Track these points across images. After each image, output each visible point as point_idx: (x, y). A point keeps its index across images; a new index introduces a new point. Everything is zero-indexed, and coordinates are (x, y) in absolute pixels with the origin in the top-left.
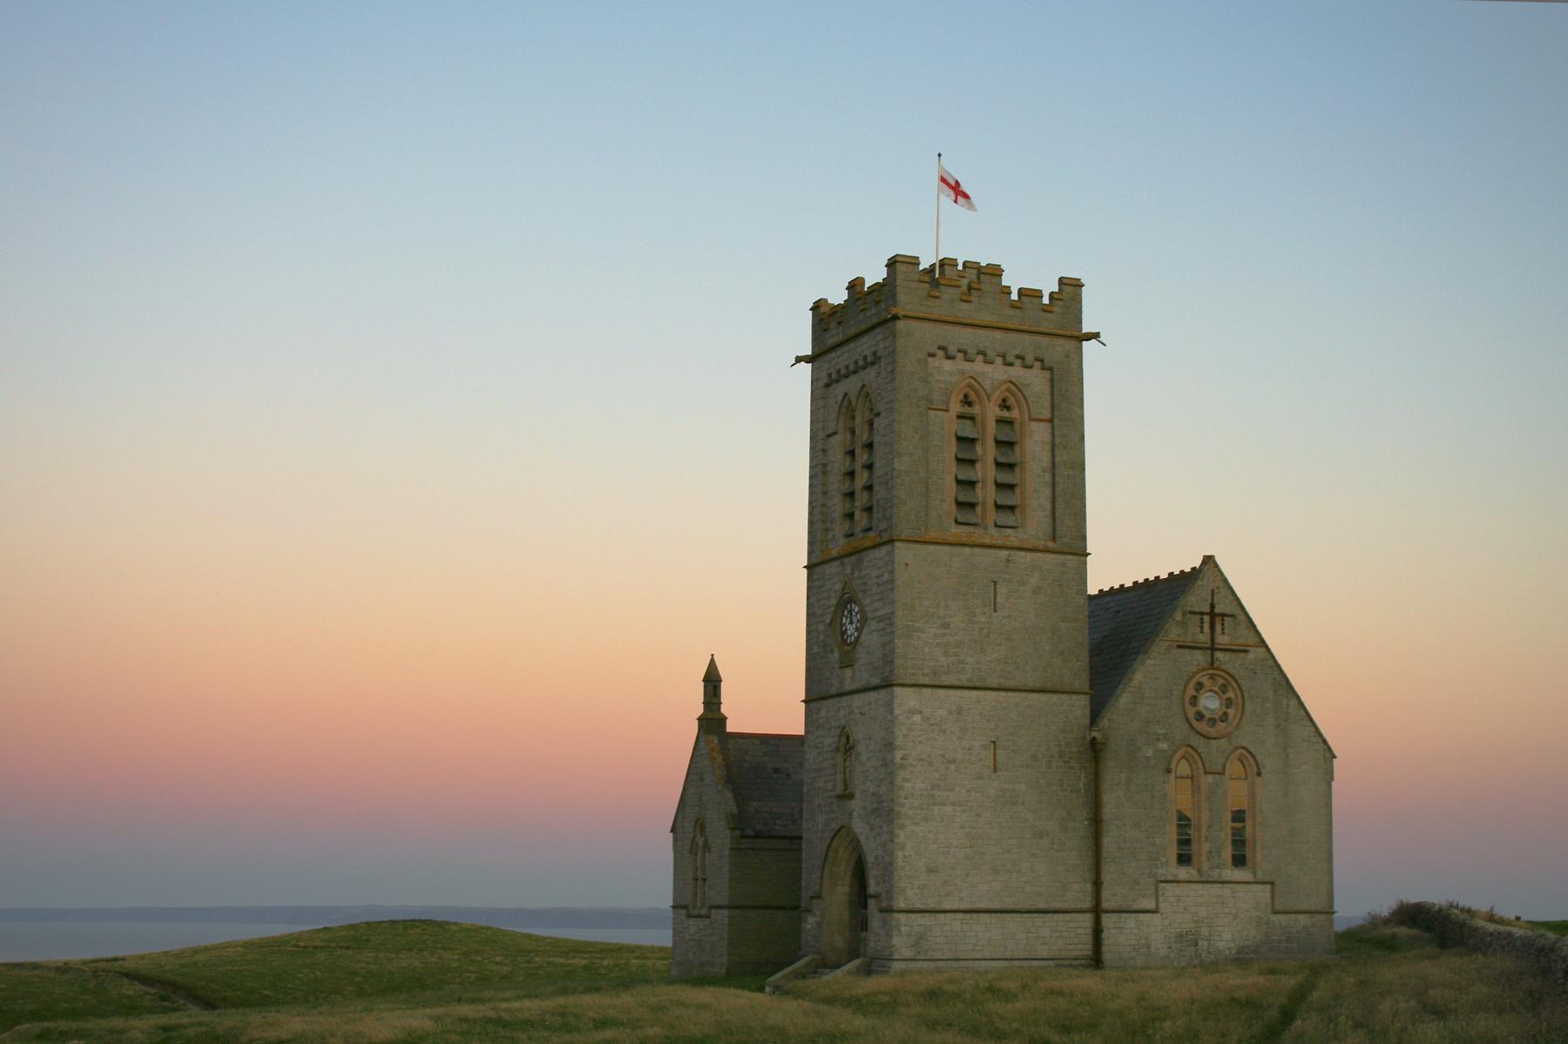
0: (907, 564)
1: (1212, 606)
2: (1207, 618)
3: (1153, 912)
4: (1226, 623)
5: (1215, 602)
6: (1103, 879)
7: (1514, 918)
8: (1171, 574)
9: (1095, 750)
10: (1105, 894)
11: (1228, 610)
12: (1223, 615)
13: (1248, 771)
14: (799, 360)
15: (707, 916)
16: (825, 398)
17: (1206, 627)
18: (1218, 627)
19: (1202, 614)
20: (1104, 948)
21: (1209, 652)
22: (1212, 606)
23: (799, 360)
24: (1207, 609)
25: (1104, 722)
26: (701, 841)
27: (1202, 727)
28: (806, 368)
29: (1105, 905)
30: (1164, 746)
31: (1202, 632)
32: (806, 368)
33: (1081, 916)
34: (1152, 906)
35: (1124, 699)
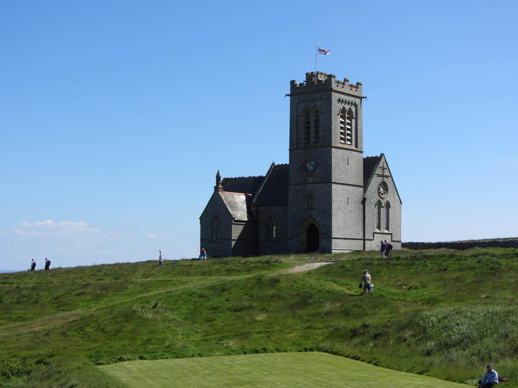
2: (382, 169)
3: (372, 240)
11: (386, 167)
12: (385, 168)
14: (287, 95)
23: (287, 95)
34: (372, 238)
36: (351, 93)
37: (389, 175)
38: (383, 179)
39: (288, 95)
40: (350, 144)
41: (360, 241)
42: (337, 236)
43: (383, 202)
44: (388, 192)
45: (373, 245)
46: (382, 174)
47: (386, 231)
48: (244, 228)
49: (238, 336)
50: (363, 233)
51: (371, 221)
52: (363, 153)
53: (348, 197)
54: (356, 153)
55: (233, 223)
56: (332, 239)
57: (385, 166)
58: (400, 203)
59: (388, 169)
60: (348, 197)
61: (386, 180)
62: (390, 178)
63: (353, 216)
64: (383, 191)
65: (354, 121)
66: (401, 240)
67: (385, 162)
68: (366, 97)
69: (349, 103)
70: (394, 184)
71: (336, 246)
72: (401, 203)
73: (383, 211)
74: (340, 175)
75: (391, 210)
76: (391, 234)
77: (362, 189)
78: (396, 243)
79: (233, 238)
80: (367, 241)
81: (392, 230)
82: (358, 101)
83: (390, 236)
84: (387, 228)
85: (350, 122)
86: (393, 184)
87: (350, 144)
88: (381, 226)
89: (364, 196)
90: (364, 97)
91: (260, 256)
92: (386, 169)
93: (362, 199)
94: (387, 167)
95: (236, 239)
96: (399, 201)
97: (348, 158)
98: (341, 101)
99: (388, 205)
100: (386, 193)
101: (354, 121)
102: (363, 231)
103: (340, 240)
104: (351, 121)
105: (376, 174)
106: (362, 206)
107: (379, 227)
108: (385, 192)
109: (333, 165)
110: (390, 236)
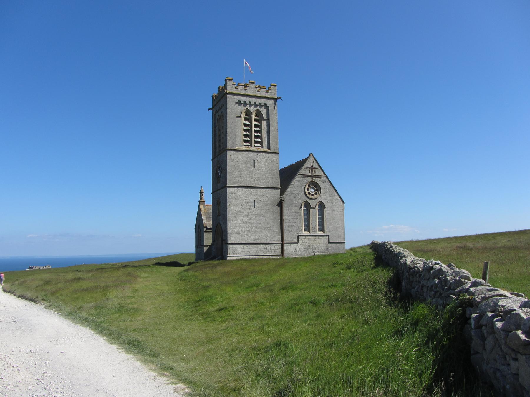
0: (230, 156)
1: (312, 166)
2: (311, 169)
3: (297, 243)
4: (316, 170)
5: (313, 165)
6: (284, 235)
7: (38, 269)
8: (303, 159)
9: (280, 204)
10: (285, 238)
11: (316, 167)
12: (315, 168)
13: (322, 207)
14: (209, 109)
15: (201, 248)
16: (460, 238)
17: (310, 171)
18: (314, 171)
19: (309, 168)
20: (285, 252)
21: (311, 178)
22: (312, 166)
23: (209, 109)
24: (310, 167)
25: (284, 195)
26: (199, 230)
27: (310, 196)
28: (211, 111)
29: (285, 241)
30: (300, 201)
31: (309, 172)
32: (211, 111)
33: (276, 246)
34: (297, 242)
35: (289, 189)
36: (259, 94)
37: (322, 174)
38: (312, 179)
39: (211, 109)
40: (260, 145)
41: (275, 245)
42: (237, 242)
43: (313, 203)
44: (320, 193)
45: (298, 249)
46: (310, 174)
47: (321, 233)
48: (212, 235)
49: (257, 323)
50: (280, 237)
51: (295, 223)
52: (279, 154)
53: (254, 201)
54: (269, 154)
55: (205, 231)
56: (228, 246)
57: (315, 165)
58: (341, 202)
59: (320, 169)
60: (254, 201)
61: (316, 180)
62: (325, 178)
63: (264, 219)
64: (315, 191)
65: (264, 123)
66: (344, 240)
67: (315, 162)
68: (280, 98)
69: (256, 105)
70: (332, 184)
71: (234, 252)
72: (344, 203)
73: (314, 214)
74: (241, 178)
75: (326, 211)
76: (329, 236)
77: (278, 191)
78: (337, 244)
79: (205, 245)
80: (285, 245)
81: (330, 231)
82: (270, 103)
83: (327, 238)
84: (322, 229)
85: (249, 123)
86: (330, 184)
87: (260, 145)
88: (311, 228)
89: (281, 198)
90: (278, 99)
91: (213, 260)
92: (317, 168)
93: (278, 202)
94: (318, 167)
95: (210, 244)
96: (341, 201)
97: (254, 160)
98: (242, 104)
99: (322, 206)
100: (319, 193)
101: (264, 123)
102: (280, 235)
103: (241, 246)
104: (261, 123)
105: (299, 175)
106: (278, 209)
107: (308, 228)
108: (317, 192)
109: (229, 168)
110: (327, 238)
